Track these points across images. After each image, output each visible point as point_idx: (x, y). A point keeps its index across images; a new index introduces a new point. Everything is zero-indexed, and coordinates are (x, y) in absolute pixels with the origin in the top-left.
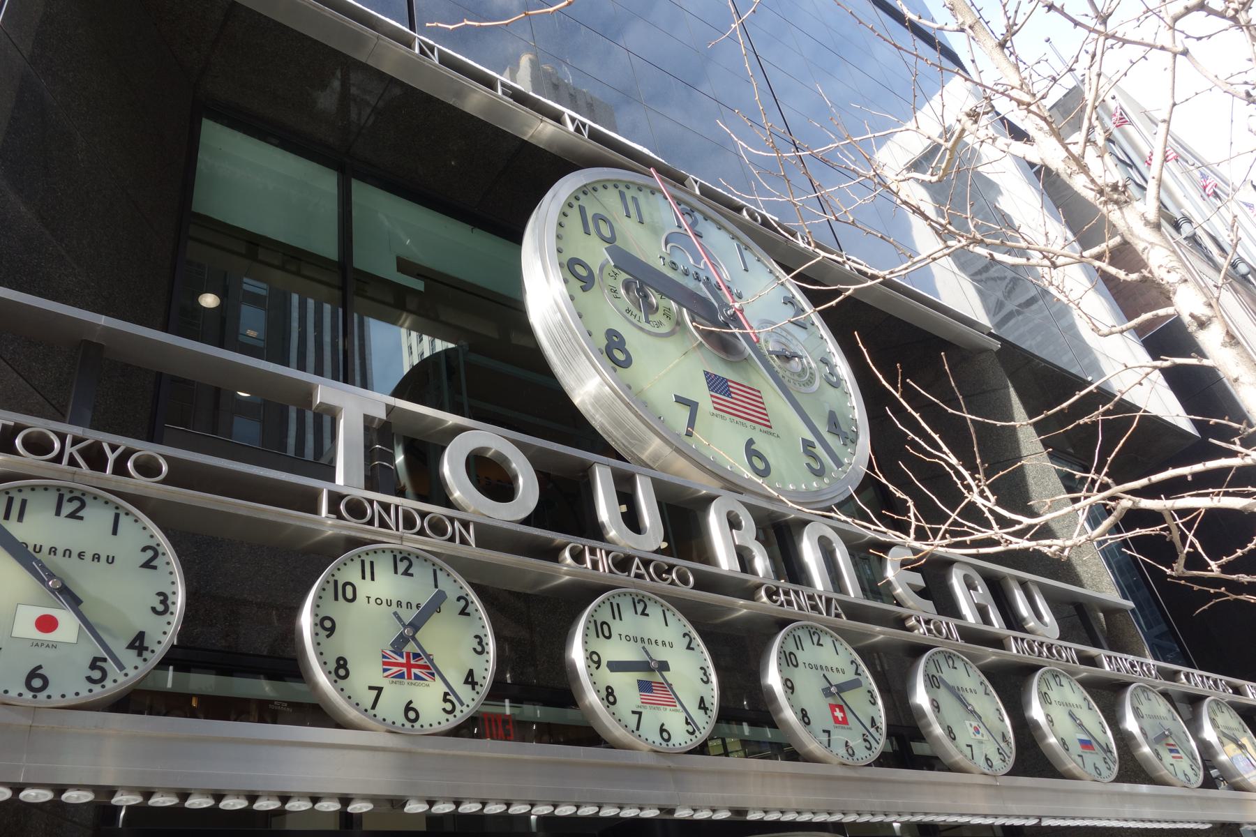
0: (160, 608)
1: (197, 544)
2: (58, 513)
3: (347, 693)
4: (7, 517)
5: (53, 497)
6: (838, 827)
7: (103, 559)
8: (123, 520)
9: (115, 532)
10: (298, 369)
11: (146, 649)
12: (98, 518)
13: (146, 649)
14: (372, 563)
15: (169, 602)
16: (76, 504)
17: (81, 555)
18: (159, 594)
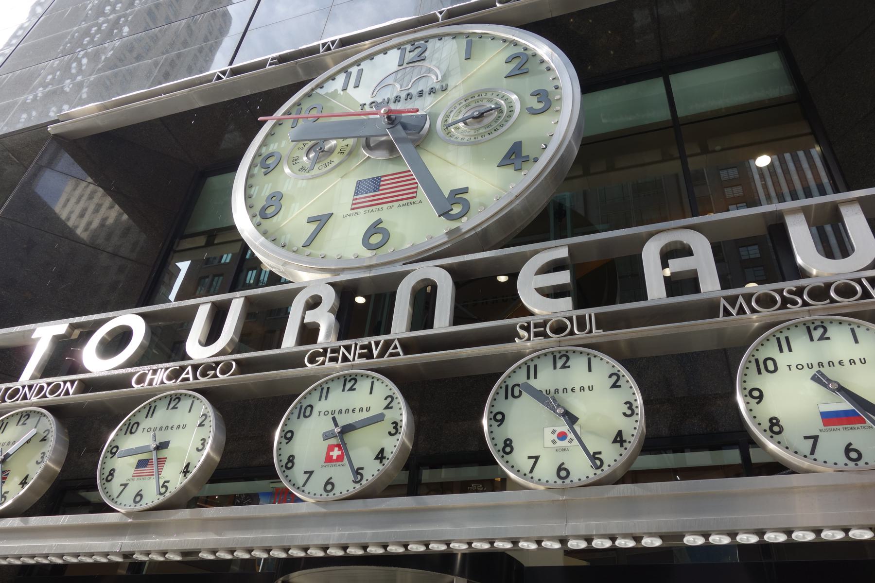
0: (629, 412)
1: (637, 363)
2: (343, 390)
3: (511, 464)
4: (528, 378)
5: (550, 358)
6: (443, 562)
7: (586, 389)
8: (593, 360)
9: (371, 393)
10: (821, 195)
11: (625, 441)
12: (578, 364)
13: (625, 441)
14: (787, 339)
15: (634, 407)
16: (564, 359)
17: (353, 411)
18: (626, 403)
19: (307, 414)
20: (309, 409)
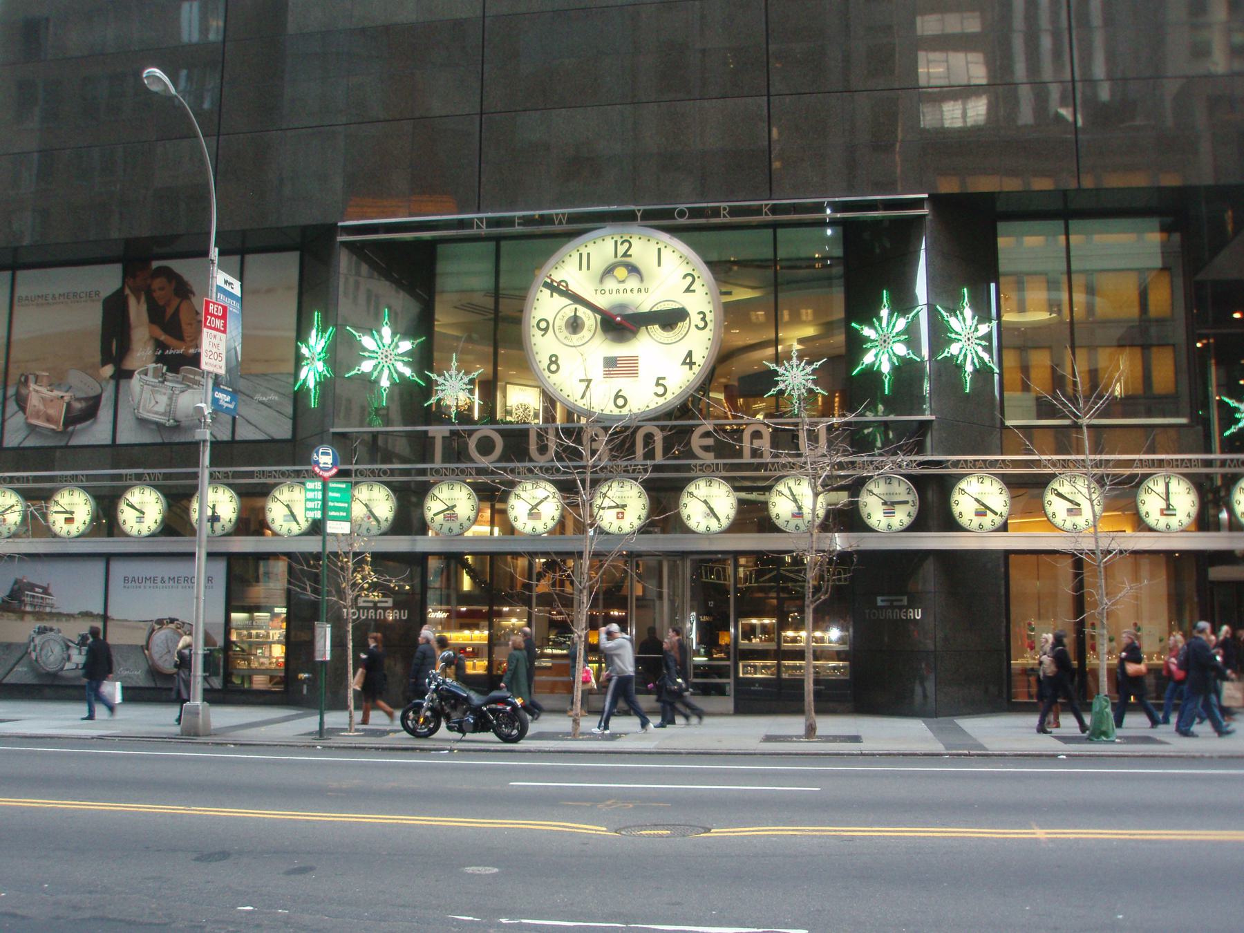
16: (627, 245)
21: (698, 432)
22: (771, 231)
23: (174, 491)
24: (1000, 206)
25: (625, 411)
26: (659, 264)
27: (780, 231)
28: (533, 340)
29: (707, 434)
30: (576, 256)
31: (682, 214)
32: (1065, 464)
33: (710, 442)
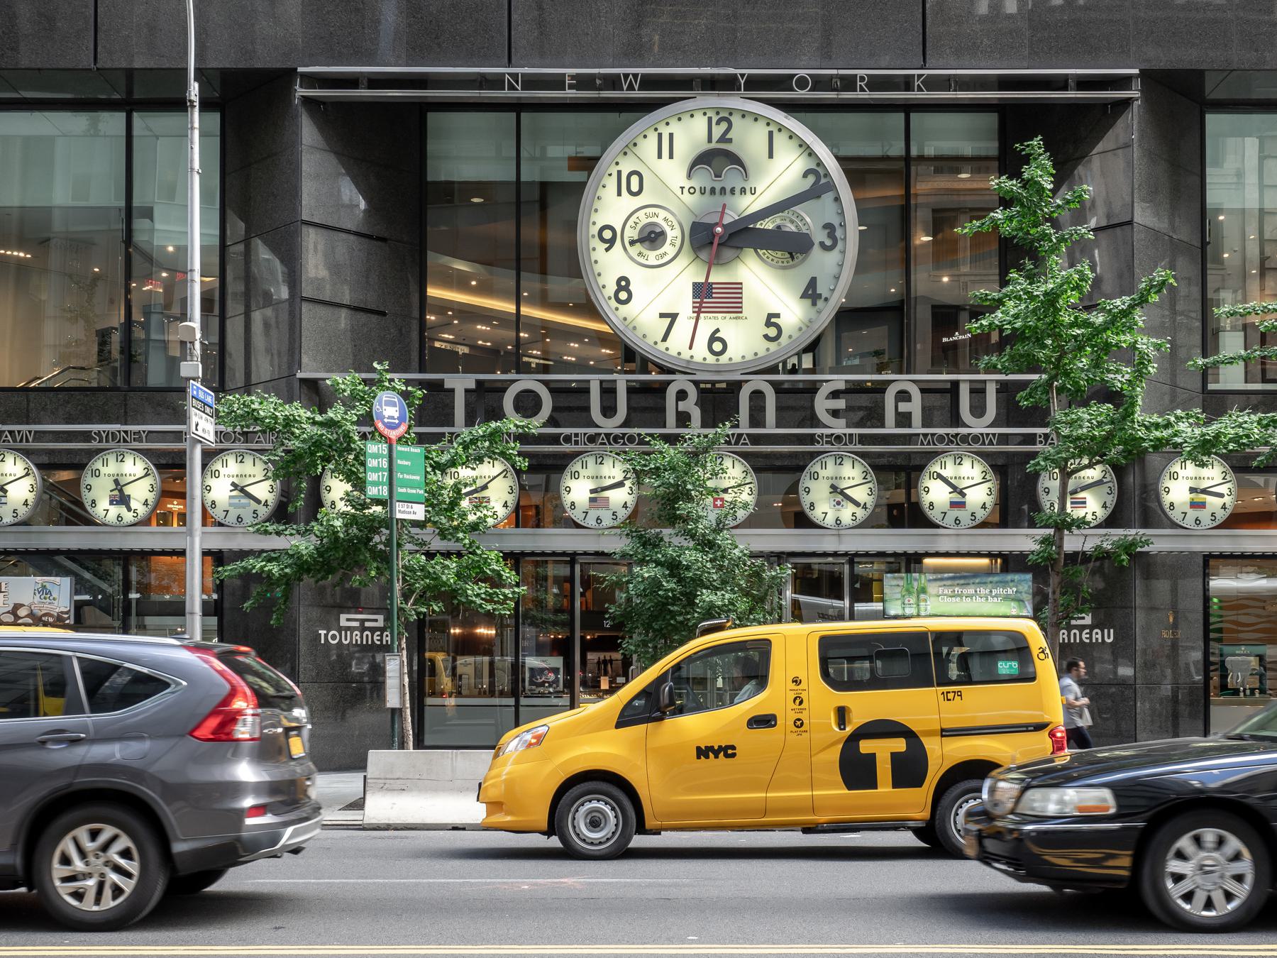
13: (820, 296)
16: (724, 126)
19: (635, 188)
20: (635, 179)
21: (825, 390)
22: (902, 115)
23: (884, 461)
24: (1213, 90)
25: (724, 359)
26: (771, 156)
27: (914, 117)
28: (594, 256)
29: (835, 395)
30: (653, 138)
31: (802, 83)
32: (951, 439)
33: (840, 404)
